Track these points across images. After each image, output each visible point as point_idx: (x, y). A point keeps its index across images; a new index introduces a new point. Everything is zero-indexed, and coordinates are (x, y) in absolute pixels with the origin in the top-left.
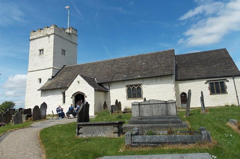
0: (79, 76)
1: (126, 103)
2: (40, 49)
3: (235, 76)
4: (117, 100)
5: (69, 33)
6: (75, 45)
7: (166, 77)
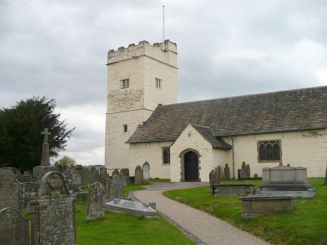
0: (190, 128)
1: (257, 168)
2: (130, 81)
4: (244, 163)
6: (174, 69)
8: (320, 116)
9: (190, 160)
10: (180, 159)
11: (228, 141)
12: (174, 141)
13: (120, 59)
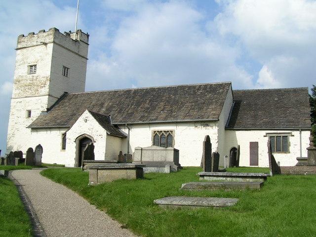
3: (302, 130)
5: (76, 41)
7: (188, 125)
8: (213, 110)
9: (85, 146)
10: (75, 144)
11: (125, 131)
12: (69, 128)
13: (29, 44)
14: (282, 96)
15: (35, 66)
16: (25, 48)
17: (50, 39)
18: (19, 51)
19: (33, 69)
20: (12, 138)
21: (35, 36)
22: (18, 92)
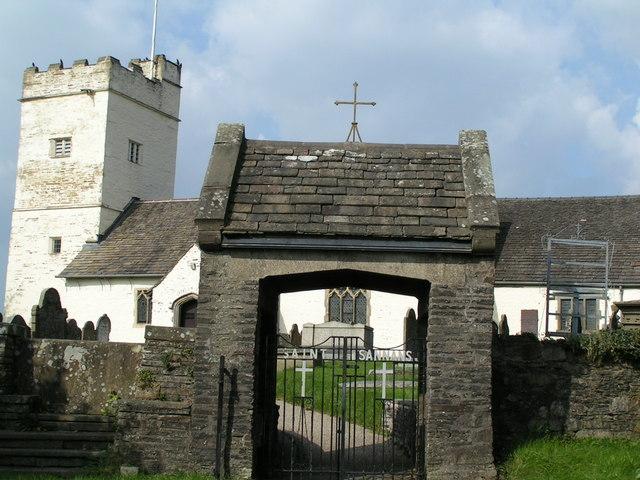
3: (624, 287)
5: (154, 82)
13: (52, 90)
14: (597, 213)
15: (68, 139)
16: (42, 98)
17: (100, 80)
18: (27, 106)
19: (63, 146)
20: (16, 298)
21: (64, 71)
22: (30, 197)
